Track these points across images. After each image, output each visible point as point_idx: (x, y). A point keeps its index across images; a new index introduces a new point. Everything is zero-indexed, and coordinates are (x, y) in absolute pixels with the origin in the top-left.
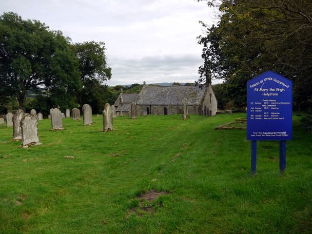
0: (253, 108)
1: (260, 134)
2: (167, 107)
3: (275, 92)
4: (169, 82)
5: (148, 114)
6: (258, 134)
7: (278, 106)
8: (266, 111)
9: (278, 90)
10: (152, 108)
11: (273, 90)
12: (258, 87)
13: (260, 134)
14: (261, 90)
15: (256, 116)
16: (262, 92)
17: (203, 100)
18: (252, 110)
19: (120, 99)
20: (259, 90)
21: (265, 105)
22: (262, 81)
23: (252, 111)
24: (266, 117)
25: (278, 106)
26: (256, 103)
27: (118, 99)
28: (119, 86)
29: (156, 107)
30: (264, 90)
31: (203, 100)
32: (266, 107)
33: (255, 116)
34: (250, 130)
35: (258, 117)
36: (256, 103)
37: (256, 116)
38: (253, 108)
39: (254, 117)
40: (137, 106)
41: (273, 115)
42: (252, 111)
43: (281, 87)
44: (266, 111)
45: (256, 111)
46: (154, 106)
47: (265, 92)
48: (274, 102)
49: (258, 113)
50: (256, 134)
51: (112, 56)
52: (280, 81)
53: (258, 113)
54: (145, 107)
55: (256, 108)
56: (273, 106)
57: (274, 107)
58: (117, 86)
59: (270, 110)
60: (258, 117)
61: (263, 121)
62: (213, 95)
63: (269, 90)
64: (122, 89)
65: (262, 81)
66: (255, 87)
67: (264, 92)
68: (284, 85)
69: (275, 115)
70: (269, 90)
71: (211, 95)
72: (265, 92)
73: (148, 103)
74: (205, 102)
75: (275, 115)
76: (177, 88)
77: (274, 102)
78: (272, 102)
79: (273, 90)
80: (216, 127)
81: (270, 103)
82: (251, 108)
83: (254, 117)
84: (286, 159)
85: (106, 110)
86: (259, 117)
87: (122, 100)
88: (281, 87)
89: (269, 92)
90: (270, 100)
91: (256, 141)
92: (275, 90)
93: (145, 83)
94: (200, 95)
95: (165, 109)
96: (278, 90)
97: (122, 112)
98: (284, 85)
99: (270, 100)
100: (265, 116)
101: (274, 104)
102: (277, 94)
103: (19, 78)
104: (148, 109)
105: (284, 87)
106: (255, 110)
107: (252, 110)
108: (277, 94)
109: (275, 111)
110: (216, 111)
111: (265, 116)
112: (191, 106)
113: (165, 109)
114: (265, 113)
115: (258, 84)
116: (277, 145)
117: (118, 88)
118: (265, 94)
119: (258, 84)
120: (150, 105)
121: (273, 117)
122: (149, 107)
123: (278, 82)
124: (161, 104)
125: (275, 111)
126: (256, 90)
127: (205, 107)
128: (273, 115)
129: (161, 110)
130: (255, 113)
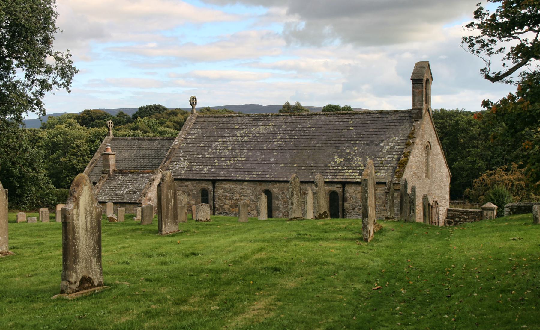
4: (265, 103)
17: (402, 165)
19: (106, 156)
28: (95, 112)
29: (236, 187)
46: (227, 186)
58: (87, 112)
62: (437, 148)
64: (110, 123)
71: (428, 148)
73: (205, 171)
76: (334, 121)
87: (112, 161)
93: (193, 101)
94: (392, 148)
97: (9, 156)
103: (401, 292)
110: (448, 207)
117: (89, 119)
120: (214, 182)
124: (254, 176)
127: (425, 198)
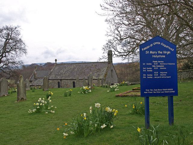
0: (145, 69)
1: (151, 91)
2: (76, 81)
3: (163, 54)
5: (59, 87)
6: (150, 91)
7: (165, 66)
8: (156, 70)
9: (165, 52)
10: (62, 82)
11: (161, 53)
12: (149, 50)
13: (151, 91)
14: (151, 52)
15: (148, 75)
16: (152, 54)
18: (144, 70)
20: (149, 52)
21: (155, 65)
22: (152, 45)
23: (144, 71)
24: (156, 76)
25: (165, 66)
26: (147, 64)
27: (33, 74)
30: (154, 53)
31: (106, 75)
32: (156, 67)
33: (147, 75)
34: (142, 90)
35: (150, 76)
36: (147, 64)
37: (148, 75)
38: (145, 69)
39: (146, 76)
40: (49, 80)
41: (162, 74)
42: (144, 71)
43: (167, 50)
44: (156, 70)
45: (148, 71)
46: (64, 81)
47: (155, 54)
48: (162, 63)
49: (150, 73)
50: (148, 91)
51: (25, 35)
52: (166, 63)
53: (150, 73)
54: (56, 82)
55: (147, 68)
56: (162, 67)
57: (162, 67)
59: (159, 70)
60: (150, 76)
61: (153, 79)
63: (158, 53)
65: (152, 45)
66: (146, 50)
67: (154, 54)
68: (170, 48)
69: (163, 74)
70: (158, 53)
72: (155, 54)
74: (107, 76)
75: (163, 74)
77: (162, 63)
78: (161, 63)
79: (161, 53)
80: (117, 95)
81: (159, 64)
82: (144, 68)
83: (146, 76)
84: (178, 85)
85: (20, 81)
86: (150, 76)
88: (167, 50)
89: (158, 54)
90: (159, 62)
91: (148, 97)
92: (163, 52)
95: (74, 83)
96: (165, 52)
98: (170, 48)
99: (159, 62)
100: (155, 75)
101: (163, 65)
102: (164, 56)
104: (59, 83)
105: (170, 50)
106: (146, 70)
107: (144, 70)
108: (164, 56)
109: (163, 71)
111: (155, 75)
112: (96, 80)
113: (74, 83)
114: (155, 73)
115: (148, 47)
116: (166, 98)
118: (155, 56)
119: (148, 47)
120: (61, 80)
121: (162, 76)
122: (60, 81)
123: (165, 46)
124: (71, 78)
125: (163, 71)
126: (147, 52)
128: (162, 74)
129: (70, 83)
130: (147, 73)
